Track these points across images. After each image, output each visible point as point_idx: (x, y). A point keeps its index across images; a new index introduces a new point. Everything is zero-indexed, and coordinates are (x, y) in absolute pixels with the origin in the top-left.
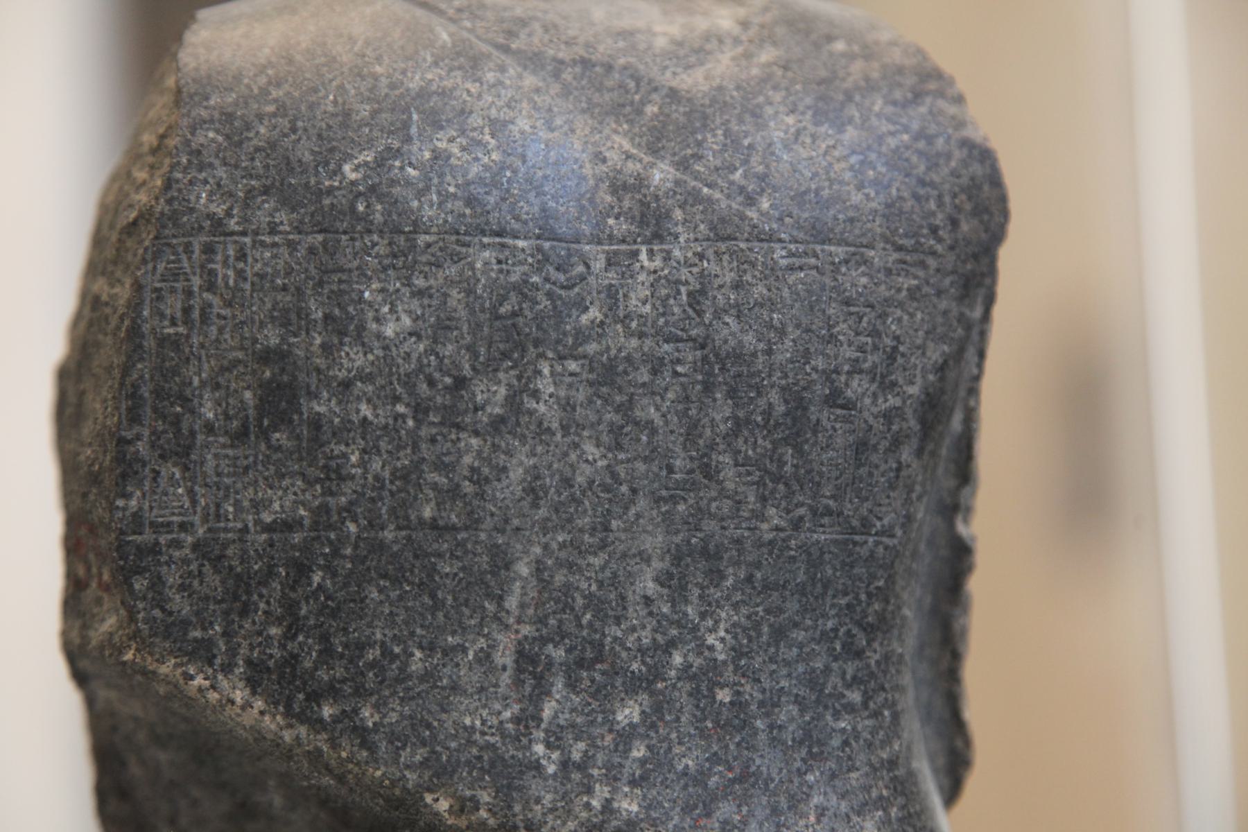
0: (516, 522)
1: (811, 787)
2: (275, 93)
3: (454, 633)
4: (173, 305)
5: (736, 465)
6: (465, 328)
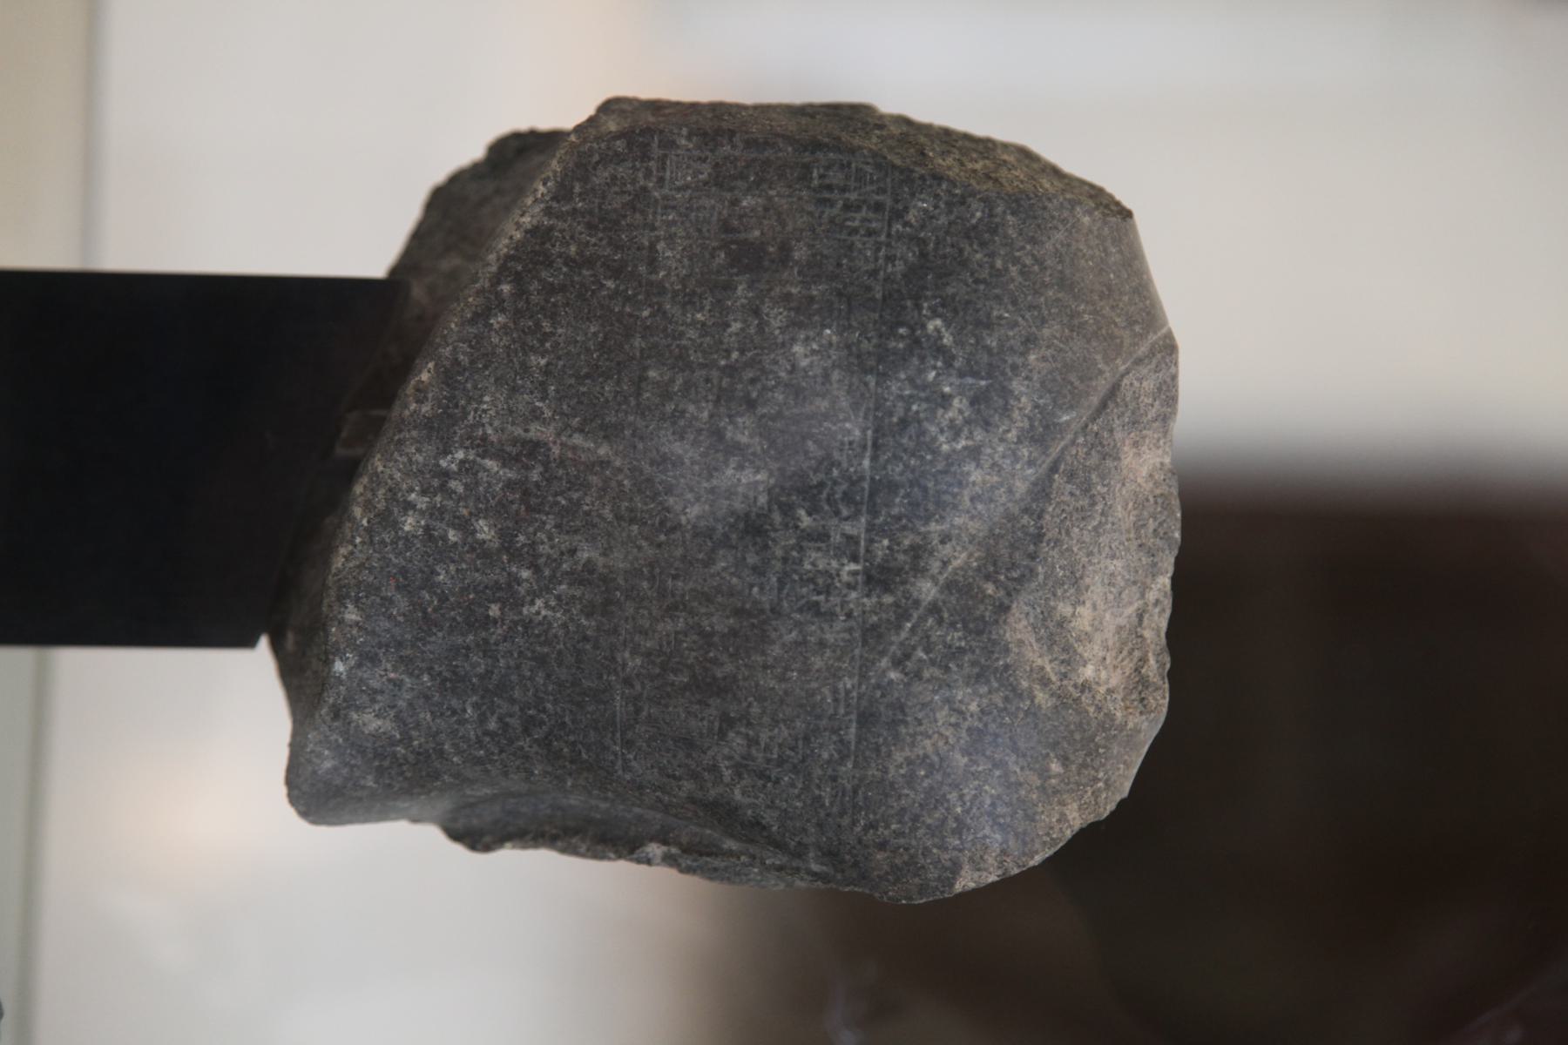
0: (640, 446)
1: (418, 677)
3: (557, 391)
4: (836, 177)
5: (677, 633)
6: (795, 411)
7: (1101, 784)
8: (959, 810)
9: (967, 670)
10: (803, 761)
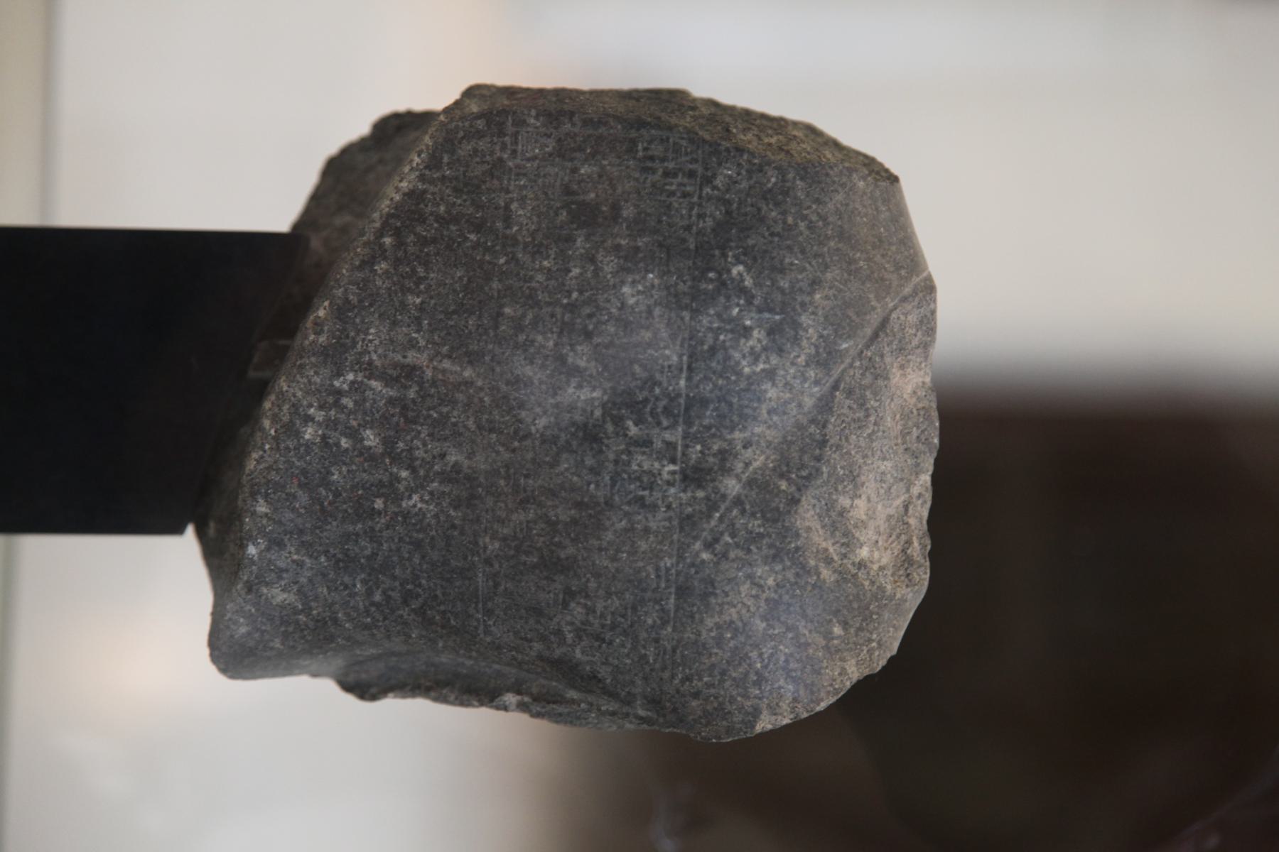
0: (498, 369)
1: (316, 558)
2: (802, 225)
3: (430, 324)
4: (657, 150)
6: (625, 340)
7: (874, 644)
8: (759, 665)
9: (765, 551)
10: (631, 626)
